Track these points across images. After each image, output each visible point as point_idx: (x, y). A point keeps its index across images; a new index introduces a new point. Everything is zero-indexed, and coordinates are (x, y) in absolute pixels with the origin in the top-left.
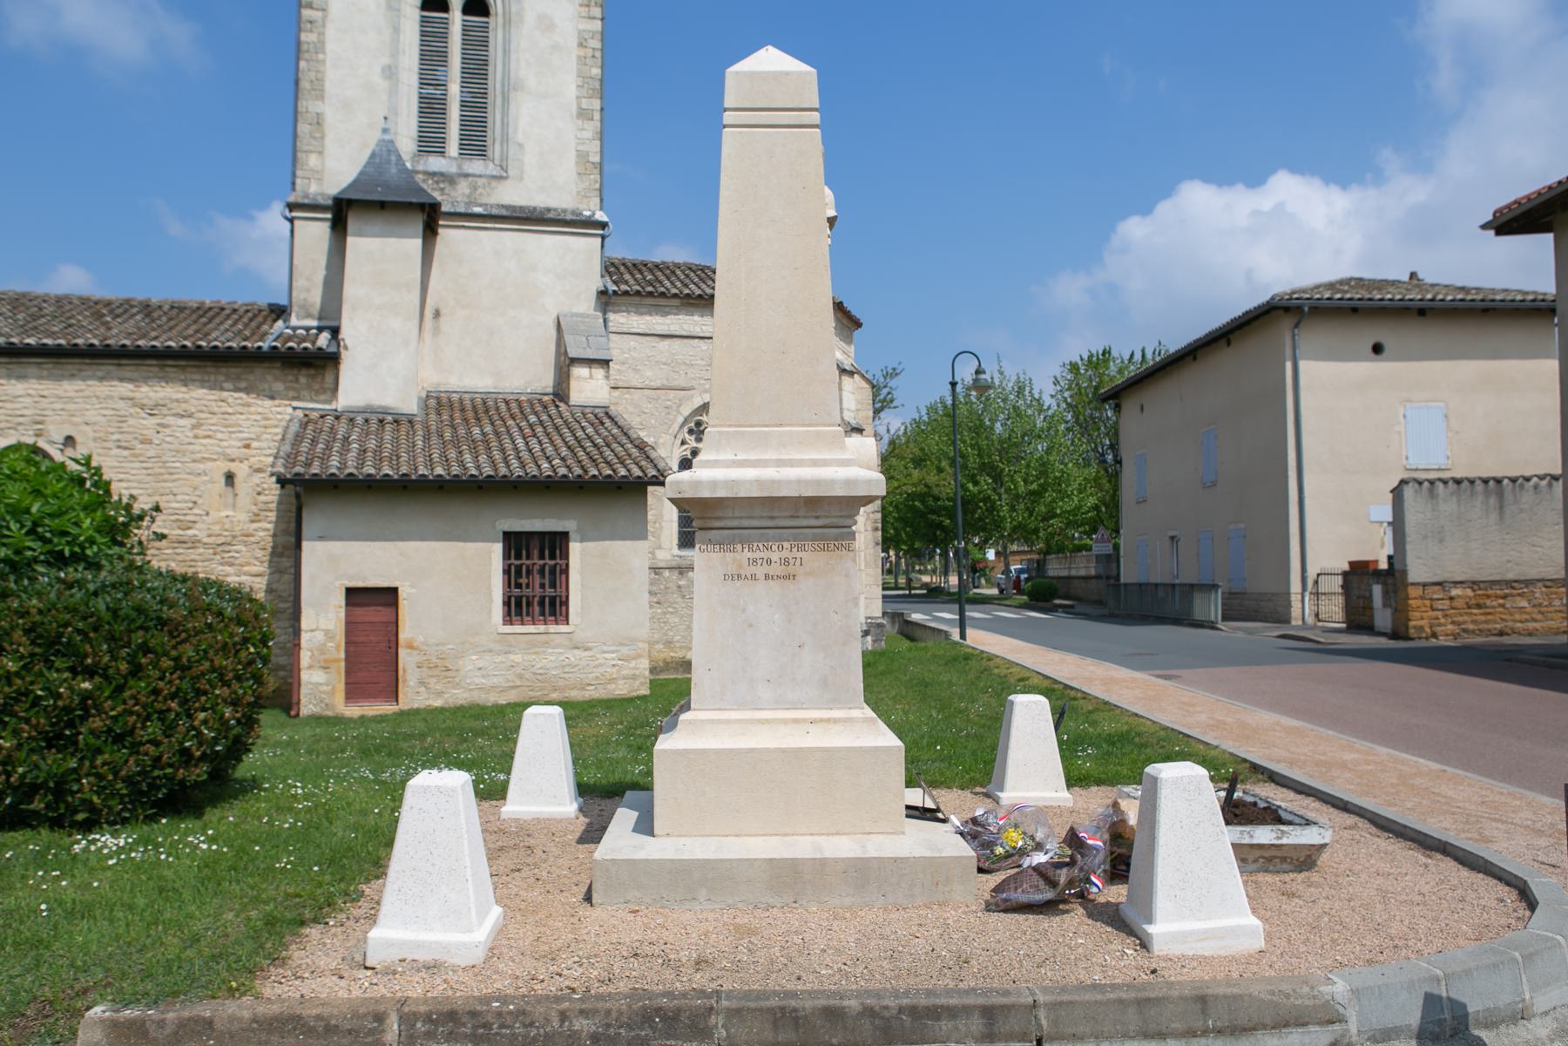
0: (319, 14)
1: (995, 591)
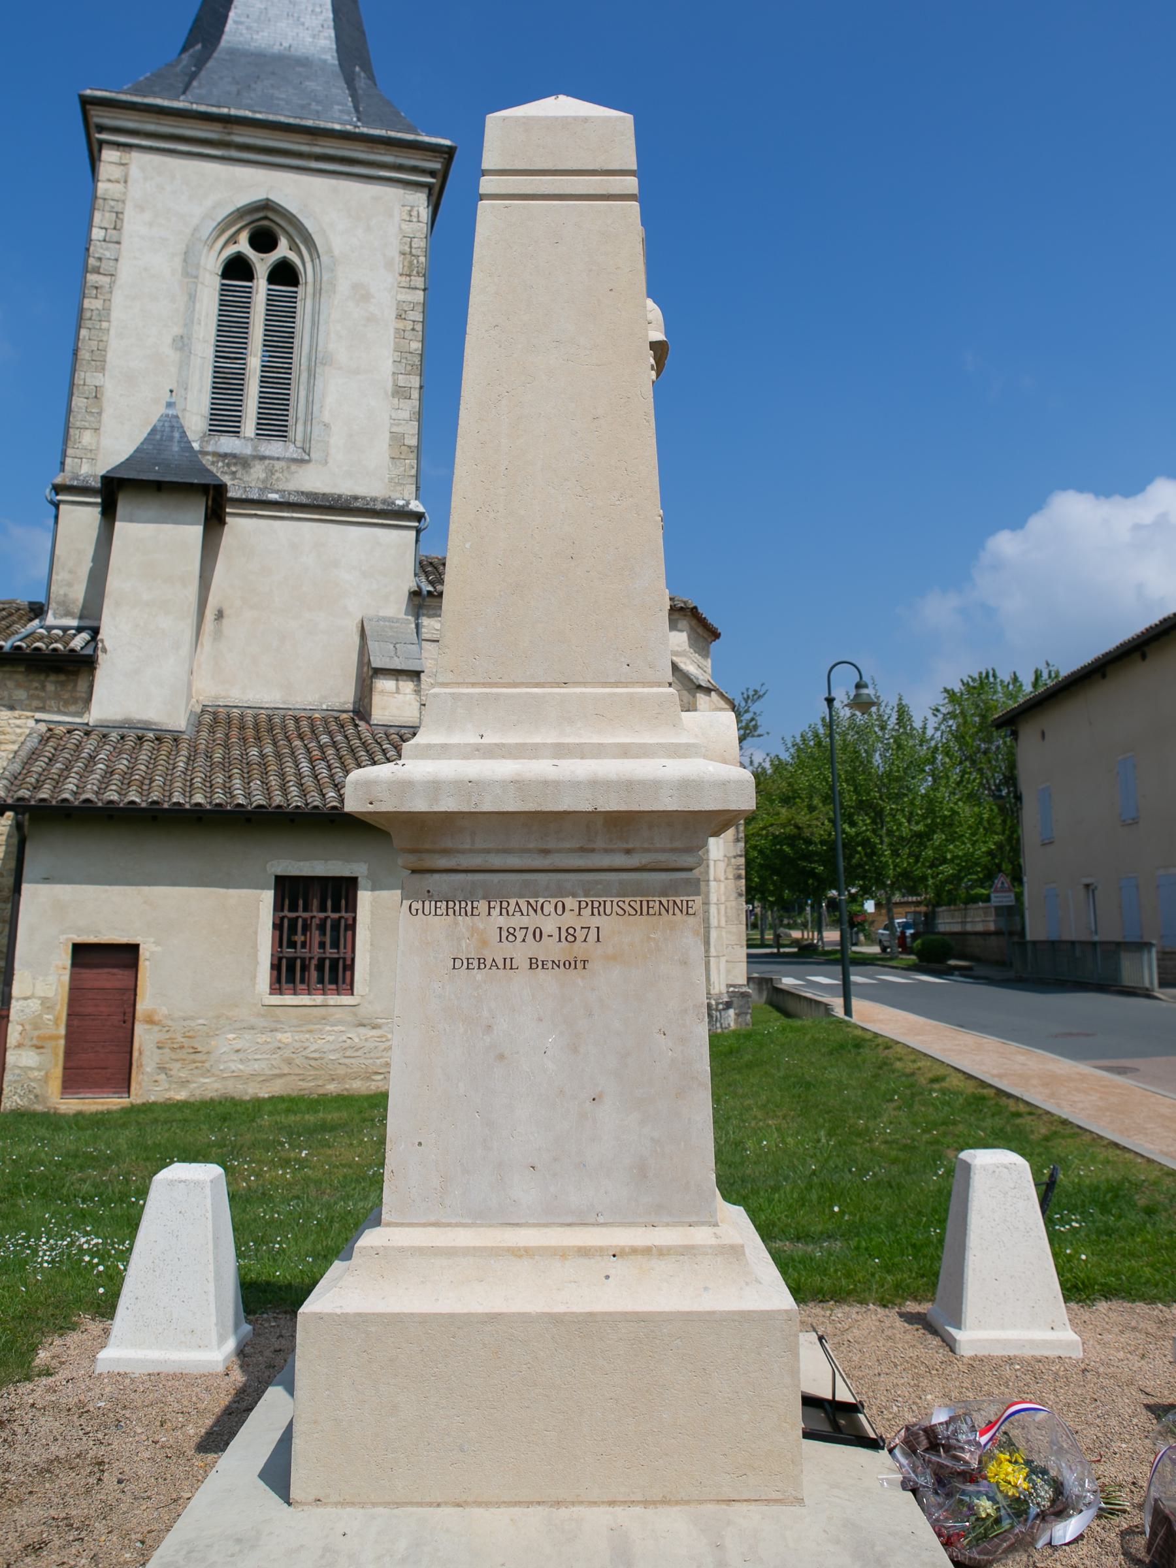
0: (107, 279)
1: (876, 949)
